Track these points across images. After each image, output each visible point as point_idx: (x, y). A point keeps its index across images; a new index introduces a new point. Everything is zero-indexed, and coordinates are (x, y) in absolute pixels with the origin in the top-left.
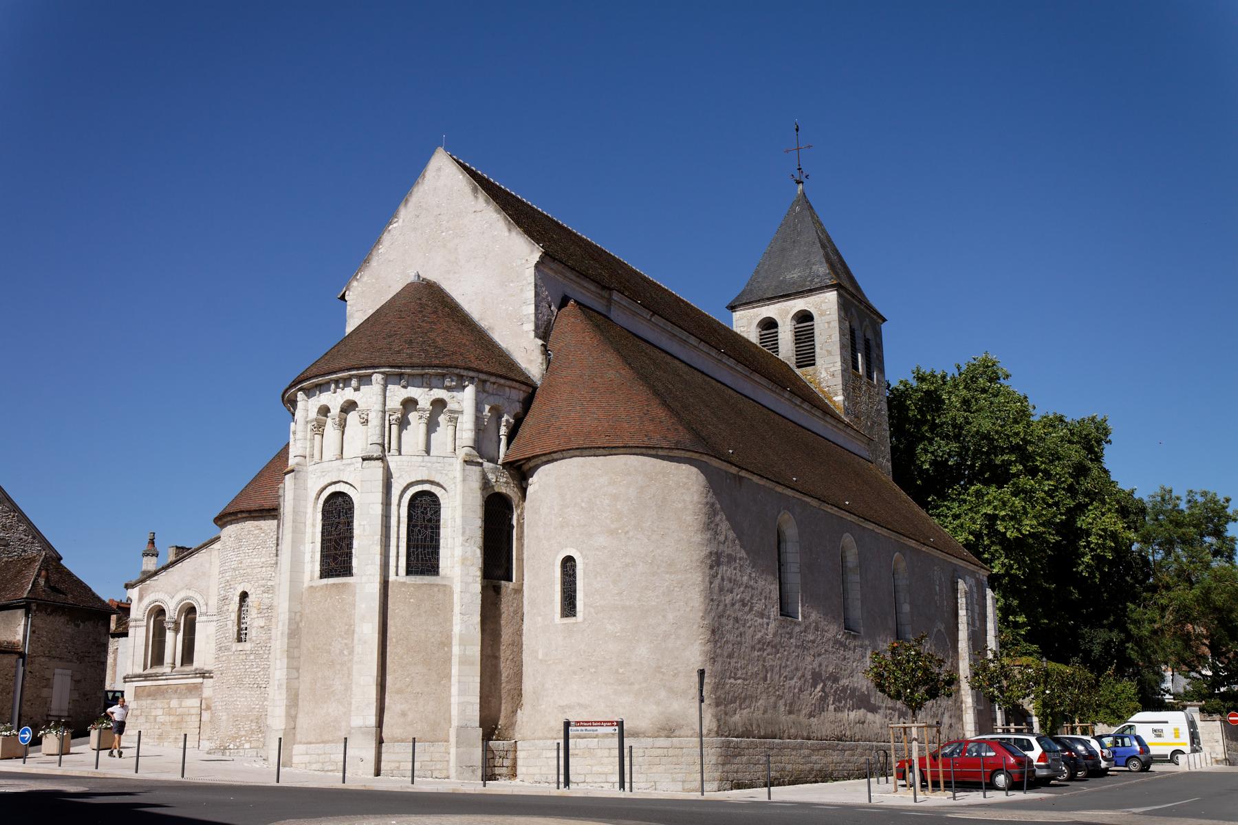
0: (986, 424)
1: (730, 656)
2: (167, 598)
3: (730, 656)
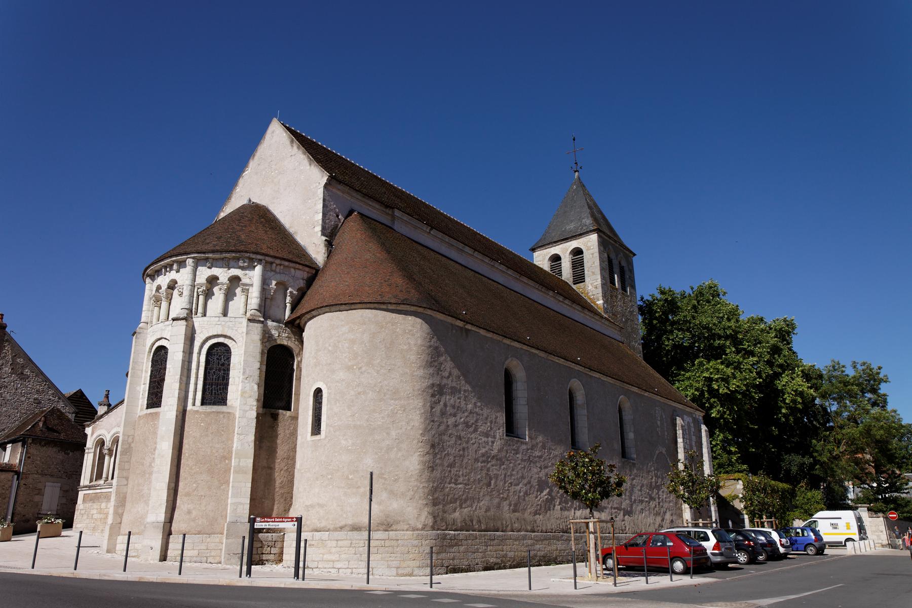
0: (704, 320)
1: (451, 465)
2: (106, 434)
3: (451, 465)
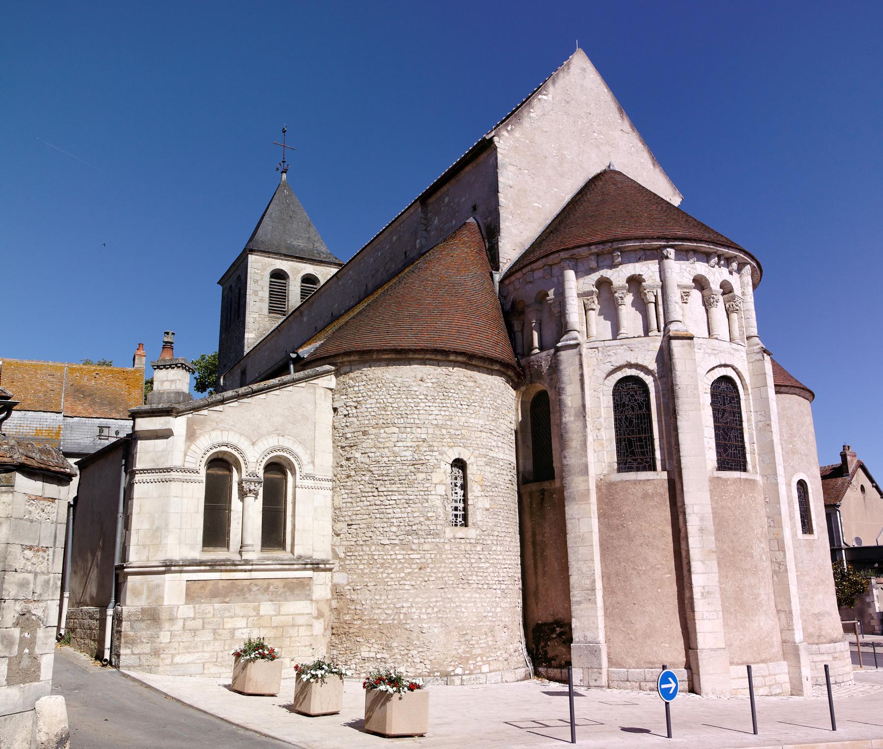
2: (243, 444)
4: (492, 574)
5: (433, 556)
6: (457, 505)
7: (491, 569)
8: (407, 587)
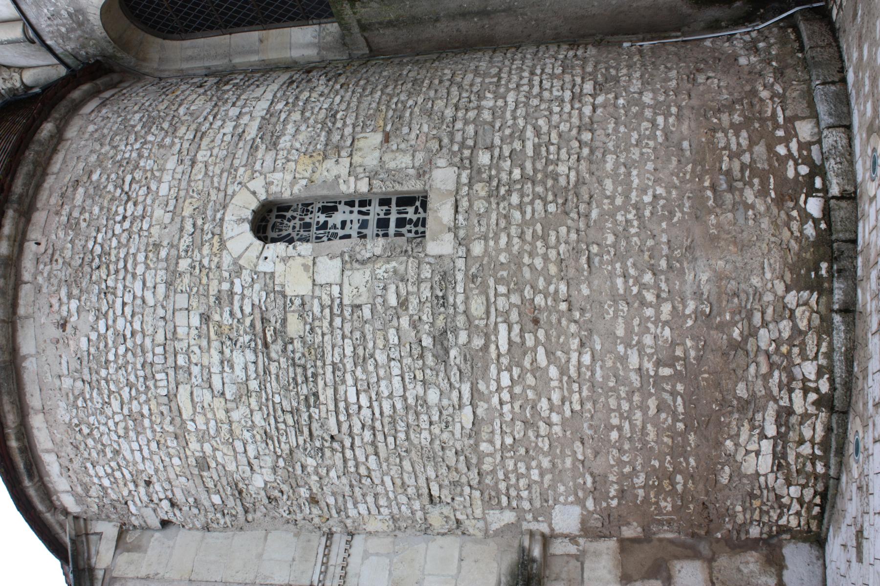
4: (555, 118)
5: (502, 289)
6: (372, 219)
7: (541, 122)
8: (587, 359)
